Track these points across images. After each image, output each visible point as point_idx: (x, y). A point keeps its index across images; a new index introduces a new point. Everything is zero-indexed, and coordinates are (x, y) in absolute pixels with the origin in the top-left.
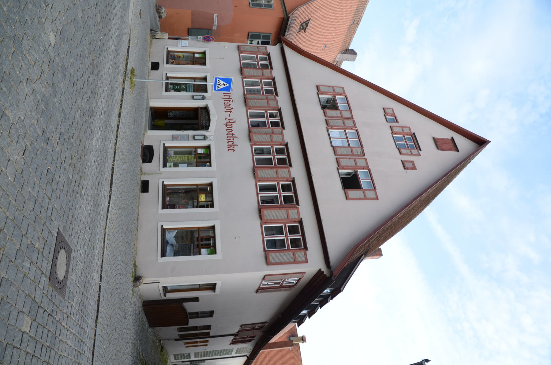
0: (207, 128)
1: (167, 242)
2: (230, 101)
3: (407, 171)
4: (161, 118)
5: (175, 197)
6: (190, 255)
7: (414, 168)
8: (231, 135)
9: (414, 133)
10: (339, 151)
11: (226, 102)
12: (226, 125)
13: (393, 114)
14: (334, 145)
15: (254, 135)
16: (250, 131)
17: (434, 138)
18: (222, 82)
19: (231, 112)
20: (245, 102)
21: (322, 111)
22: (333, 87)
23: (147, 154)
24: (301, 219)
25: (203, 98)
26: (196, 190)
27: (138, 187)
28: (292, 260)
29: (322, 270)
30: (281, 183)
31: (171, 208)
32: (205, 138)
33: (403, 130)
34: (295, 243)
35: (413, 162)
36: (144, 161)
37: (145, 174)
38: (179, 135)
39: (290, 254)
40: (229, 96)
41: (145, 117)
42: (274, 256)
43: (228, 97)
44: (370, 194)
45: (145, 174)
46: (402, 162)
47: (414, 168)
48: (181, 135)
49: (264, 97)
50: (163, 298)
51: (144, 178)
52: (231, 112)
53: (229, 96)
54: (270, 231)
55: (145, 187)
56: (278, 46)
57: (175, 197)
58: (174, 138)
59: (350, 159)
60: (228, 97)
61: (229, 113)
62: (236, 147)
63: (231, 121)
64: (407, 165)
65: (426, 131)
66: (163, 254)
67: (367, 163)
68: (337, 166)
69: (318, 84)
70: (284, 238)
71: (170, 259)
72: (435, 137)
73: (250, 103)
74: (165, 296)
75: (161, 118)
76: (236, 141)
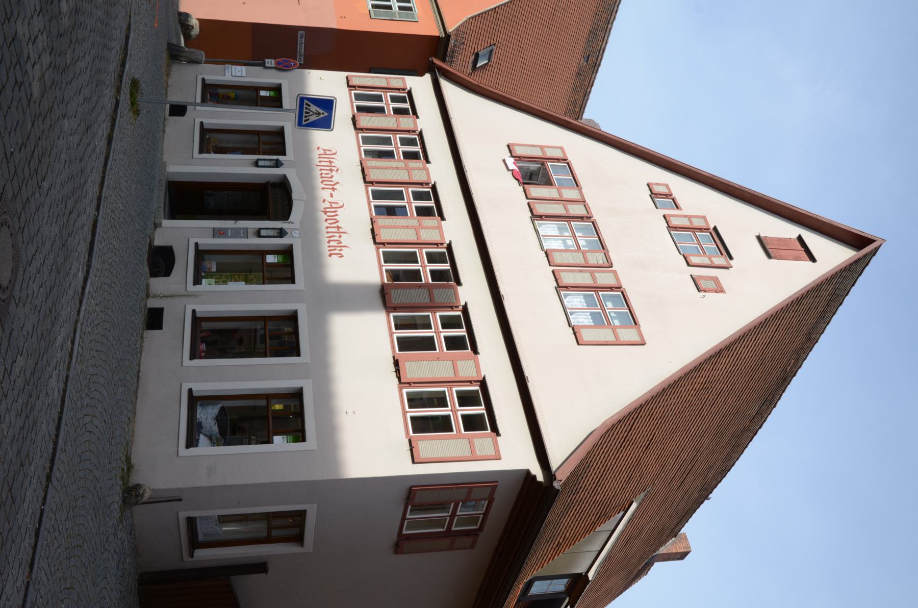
0: (285, 214)
1: (200, 425)
2: (331, 170)
3: (702, 294)
4: (189, 199)
5: (219, 338)
6: (250, 443)
7: (720, 290)
8: (336, 230)
9: (715, 229)
10: (557, 258)
13: (668, 196)
14: (574, 322)
15: (420, 443)
16: (396, 363)
17: (759, 238)
18: (314, 108)
19: (334, 189)
20: (398, 371)
21: (521, 188)
22: (542, 148)
23: (162, 261)
24: (484, 378)
25: (278, 164)
26: (267, 417)
27: (140, 319)
29: (533, 472)
32: (281, 233)
33: (690, 222)
34: (472, 423)
35: (716, 280)
36: (154, 274)
37: (155, 296)
38: (227, 229)
40: (330, 162)
41: (159, 197)
44: (628, 334)
45: (155, 296)
46: (664, 216)
47: (720, 290)
48: (231, 229)
49: (402, 165)
50: (188, 562)
51: (153, 303)
52: (334, 189)
53: (330, 162)
54: (415, 401)
55: (155, 319)
56: (428, 77)
57: (219, 338)
58: (217, 233)
59: (581, 271)
60: (328, 164)
61: (331, 191)
62: (345, 252)
63: (334, 205)
64: (703, 284)
65: (742, 224)
66: (191, 442)
67: (617, 279)
68: (555, 285)
69: (511, 141)
71: (204, 448)
72: (762, 235)
74: (192, 555)
75: (189, 199)
76: (345, 240)
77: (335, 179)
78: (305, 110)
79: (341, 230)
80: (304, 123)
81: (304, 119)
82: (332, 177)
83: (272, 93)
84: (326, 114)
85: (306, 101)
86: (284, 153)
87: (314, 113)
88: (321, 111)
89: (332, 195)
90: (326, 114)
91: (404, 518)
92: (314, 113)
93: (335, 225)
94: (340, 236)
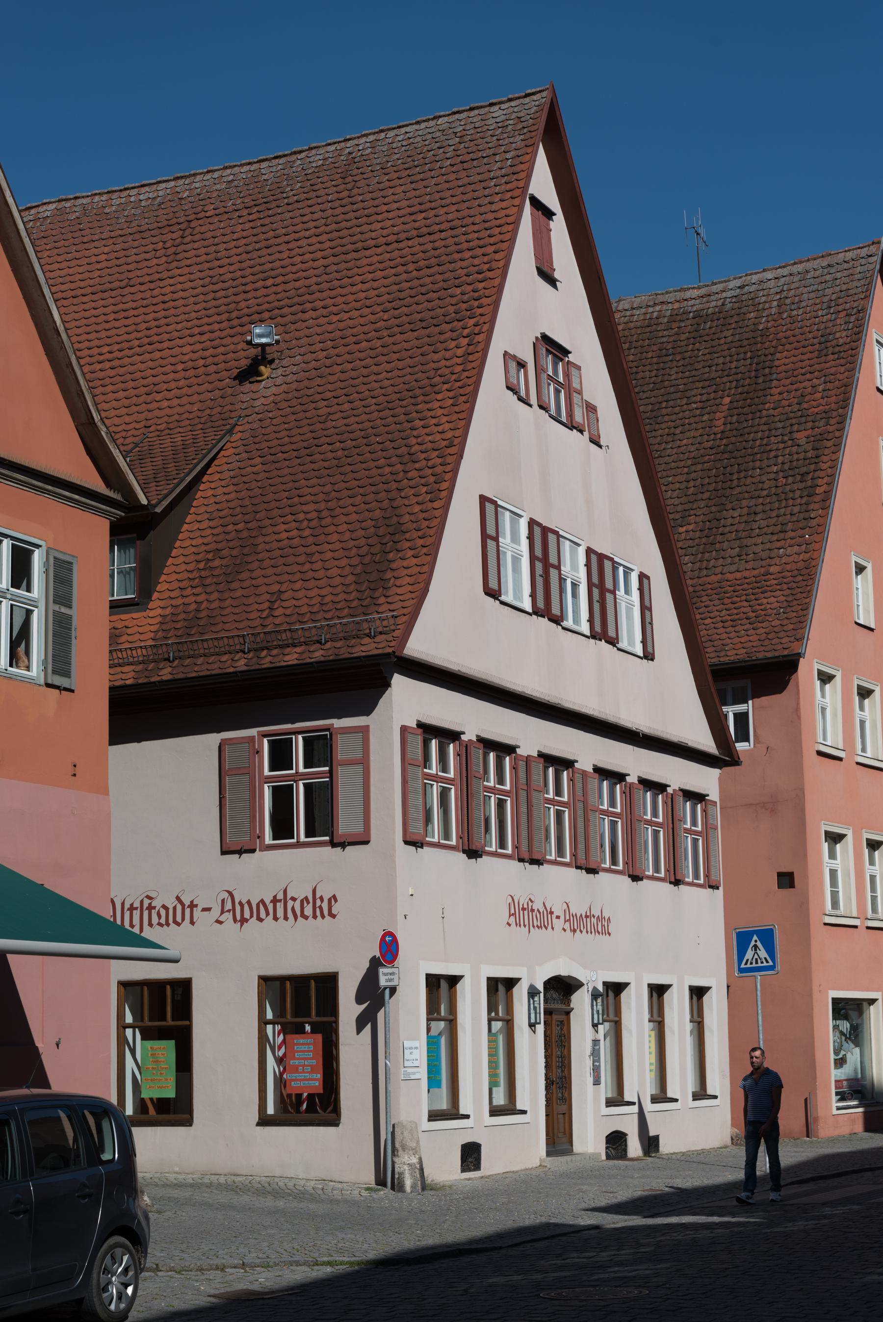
11: (155, 920)
12: (244, 921)
18: (749, 954)
19: (192, 906)
28: (359, 768)
30: (266, 772)
31: (490, 1062)
39: (342, 773)
40: (132, 908)
42: (346, 823)
43: (136, 914)
52: (192, 906)
60: (136, 914)
61: (197, 912)
63: (228, 906)
70: (301, 784)
73: (244, 840)
76: (299, 891)
77: (171, 903)
78: (754, 965)
79: (280, 896)
80: (771, 963)
81: (765, 964)
82: (164, 907)
83: (599, 1000)
84: (755, 938)
85: (743, 966)
86: (327, 984)
87: (756, 953)
88: (753, 943)
89: (208, 909)
90: (755, 938)
91: (554, 863)
92: (756, 953)
93: (271, 907)
94: (294, 899)
